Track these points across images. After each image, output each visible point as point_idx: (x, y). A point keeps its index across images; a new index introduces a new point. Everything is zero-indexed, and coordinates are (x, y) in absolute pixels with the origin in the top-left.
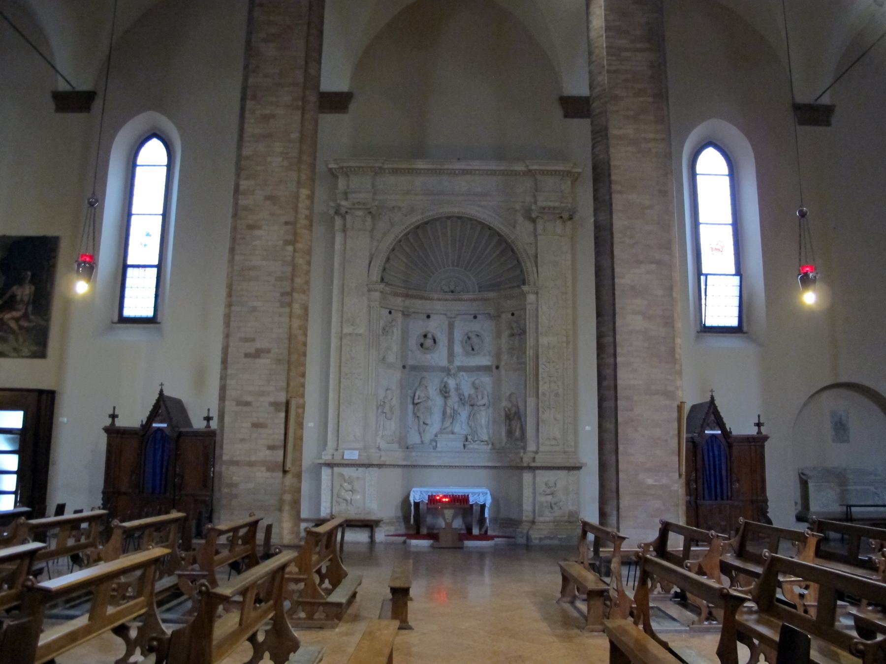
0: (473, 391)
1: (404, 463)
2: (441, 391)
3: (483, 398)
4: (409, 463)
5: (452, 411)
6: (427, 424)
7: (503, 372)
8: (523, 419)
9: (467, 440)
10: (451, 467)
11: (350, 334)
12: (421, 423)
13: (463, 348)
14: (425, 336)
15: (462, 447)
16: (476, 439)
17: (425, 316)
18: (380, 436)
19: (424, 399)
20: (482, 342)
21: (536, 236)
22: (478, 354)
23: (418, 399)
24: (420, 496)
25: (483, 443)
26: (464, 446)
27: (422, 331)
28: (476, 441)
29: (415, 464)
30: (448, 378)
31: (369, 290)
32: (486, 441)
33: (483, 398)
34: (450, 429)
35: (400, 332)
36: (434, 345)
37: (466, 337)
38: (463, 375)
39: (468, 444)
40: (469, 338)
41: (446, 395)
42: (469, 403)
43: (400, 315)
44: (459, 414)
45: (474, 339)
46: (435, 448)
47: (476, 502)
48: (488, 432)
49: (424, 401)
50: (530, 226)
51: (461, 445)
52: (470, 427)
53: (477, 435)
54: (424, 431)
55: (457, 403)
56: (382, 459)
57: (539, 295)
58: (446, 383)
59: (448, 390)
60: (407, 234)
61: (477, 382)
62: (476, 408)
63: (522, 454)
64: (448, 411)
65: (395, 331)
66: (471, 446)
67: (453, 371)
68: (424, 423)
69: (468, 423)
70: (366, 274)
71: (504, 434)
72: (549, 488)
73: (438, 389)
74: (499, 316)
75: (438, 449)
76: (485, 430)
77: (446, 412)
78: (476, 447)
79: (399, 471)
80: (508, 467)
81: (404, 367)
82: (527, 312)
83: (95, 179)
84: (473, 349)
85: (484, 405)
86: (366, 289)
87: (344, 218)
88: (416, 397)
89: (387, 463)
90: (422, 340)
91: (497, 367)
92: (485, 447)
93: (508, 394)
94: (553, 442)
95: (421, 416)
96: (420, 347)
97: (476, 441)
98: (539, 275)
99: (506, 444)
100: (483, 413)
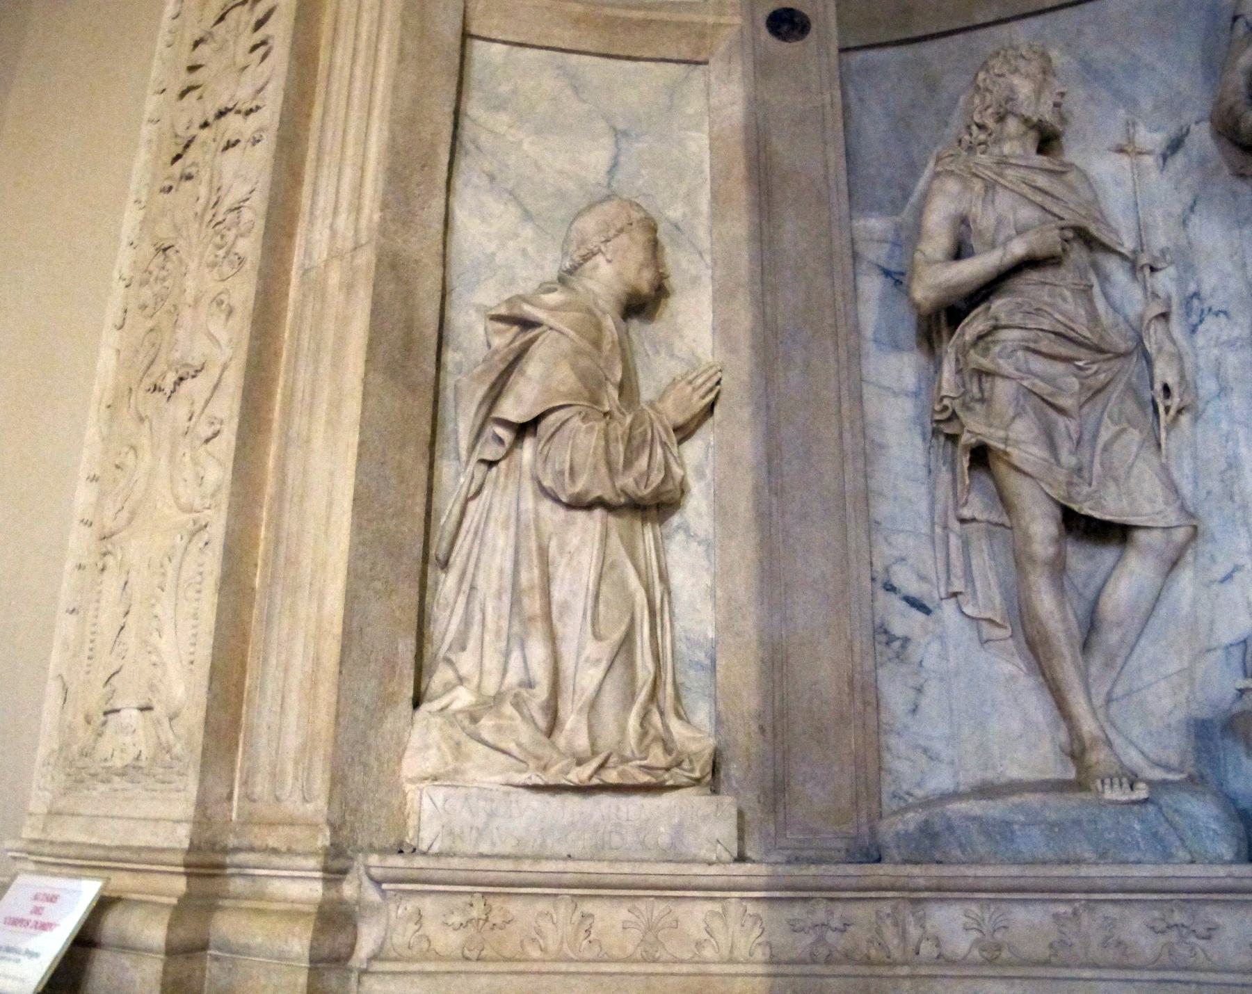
19: (1018, 249)
23: (959, 252)
54: (1091, 626)
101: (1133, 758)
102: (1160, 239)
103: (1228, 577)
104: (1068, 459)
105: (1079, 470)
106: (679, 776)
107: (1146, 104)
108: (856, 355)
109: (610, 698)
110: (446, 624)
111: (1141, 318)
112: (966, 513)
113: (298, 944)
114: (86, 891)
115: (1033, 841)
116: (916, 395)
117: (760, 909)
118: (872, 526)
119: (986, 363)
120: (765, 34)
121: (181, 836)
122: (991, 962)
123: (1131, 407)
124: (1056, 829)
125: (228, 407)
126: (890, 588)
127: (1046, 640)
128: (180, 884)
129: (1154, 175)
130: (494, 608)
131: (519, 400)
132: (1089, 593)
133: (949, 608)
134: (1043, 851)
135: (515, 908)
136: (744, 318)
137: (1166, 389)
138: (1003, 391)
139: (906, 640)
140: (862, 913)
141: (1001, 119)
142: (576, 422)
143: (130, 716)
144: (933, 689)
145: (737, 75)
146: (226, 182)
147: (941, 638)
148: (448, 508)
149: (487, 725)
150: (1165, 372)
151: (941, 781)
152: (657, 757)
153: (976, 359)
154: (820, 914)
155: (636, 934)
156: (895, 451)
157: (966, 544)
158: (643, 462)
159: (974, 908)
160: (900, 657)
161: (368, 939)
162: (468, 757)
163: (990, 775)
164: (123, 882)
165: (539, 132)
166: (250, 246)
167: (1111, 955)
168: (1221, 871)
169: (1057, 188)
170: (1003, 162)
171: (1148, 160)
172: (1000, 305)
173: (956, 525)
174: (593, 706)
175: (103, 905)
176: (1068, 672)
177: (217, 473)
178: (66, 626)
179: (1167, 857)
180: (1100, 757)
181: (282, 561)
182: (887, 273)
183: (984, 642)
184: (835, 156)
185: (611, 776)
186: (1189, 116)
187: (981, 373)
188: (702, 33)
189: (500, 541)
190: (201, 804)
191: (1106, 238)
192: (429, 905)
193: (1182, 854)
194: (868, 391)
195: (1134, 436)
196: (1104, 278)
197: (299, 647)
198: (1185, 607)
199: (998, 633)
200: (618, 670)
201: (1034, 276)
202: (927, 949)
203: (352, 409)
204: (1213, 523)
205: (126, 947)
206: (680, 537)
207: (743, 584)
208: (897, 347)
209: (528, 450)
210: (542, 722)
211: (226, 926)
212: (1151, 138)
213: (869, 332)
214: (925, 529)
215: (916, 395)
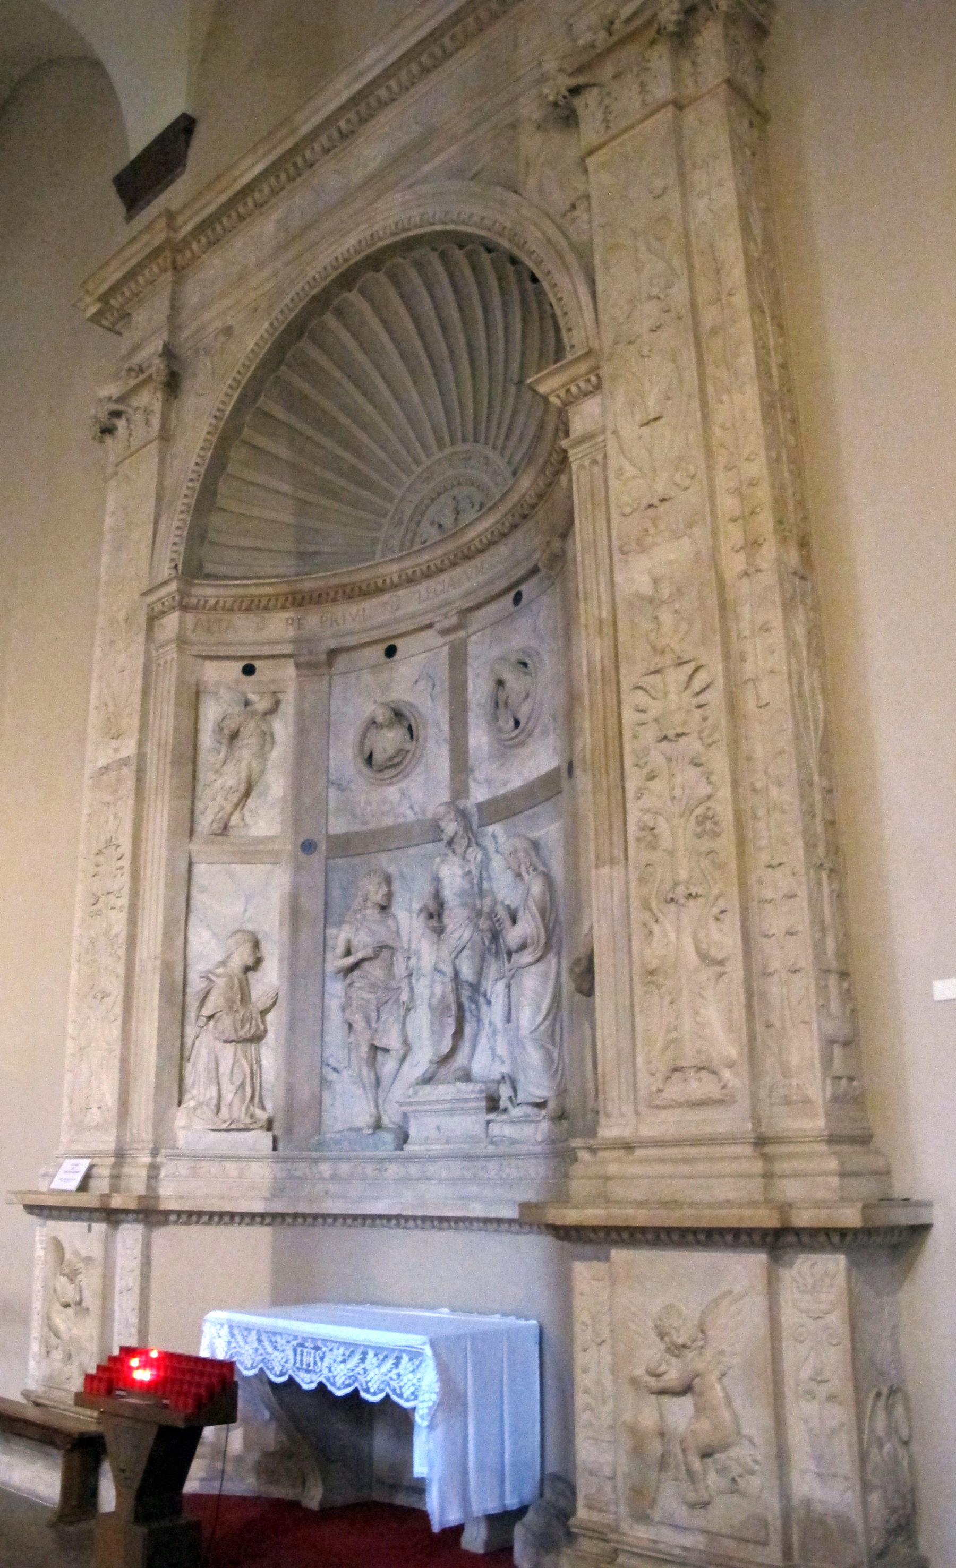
10: (442, 1222)
24: (229, 1343)
38: (494, 836)
43: (289, 671)
47: (387, 1397)
72: (677, 1350)
79: (262, 1234)
80: (263, 1216)
81: (308, 847)
94: (698, 1087)
98: (601, 305)
106: (255, 1126)
109: (237, 1102)
110: (189, 1080)
113: (144, 1173)
114: (84, 1164)
115: (346, 1144)
120: (300, 853)
121: (112, 1146)
125: (118, 1010)
126: (328, 1065)
128: (113, 1160)
130: (203, 1076)
135: (203, 1163)
143: (94, 1110)
148: (189, 1041)
149: (198, 1112)
152: (248, 1120)
158: (248, 1026)
161: (163, 1173)
164: (96, 1161)
166: (122, 952)
171: (415, 915)
174: (231, 1105)
175: (91, 1167)
177: (116, 1032)
178: (68, 1077)
185: (233, 1126)
189: (204, 1052)
190: (118, 1137)
192: (179, 1163)
200: (239, 1094)
203: (156, 1015)
205: (100, 1177)
209: (212, 1023)
211: (126, 1170)
212: (416, 906)
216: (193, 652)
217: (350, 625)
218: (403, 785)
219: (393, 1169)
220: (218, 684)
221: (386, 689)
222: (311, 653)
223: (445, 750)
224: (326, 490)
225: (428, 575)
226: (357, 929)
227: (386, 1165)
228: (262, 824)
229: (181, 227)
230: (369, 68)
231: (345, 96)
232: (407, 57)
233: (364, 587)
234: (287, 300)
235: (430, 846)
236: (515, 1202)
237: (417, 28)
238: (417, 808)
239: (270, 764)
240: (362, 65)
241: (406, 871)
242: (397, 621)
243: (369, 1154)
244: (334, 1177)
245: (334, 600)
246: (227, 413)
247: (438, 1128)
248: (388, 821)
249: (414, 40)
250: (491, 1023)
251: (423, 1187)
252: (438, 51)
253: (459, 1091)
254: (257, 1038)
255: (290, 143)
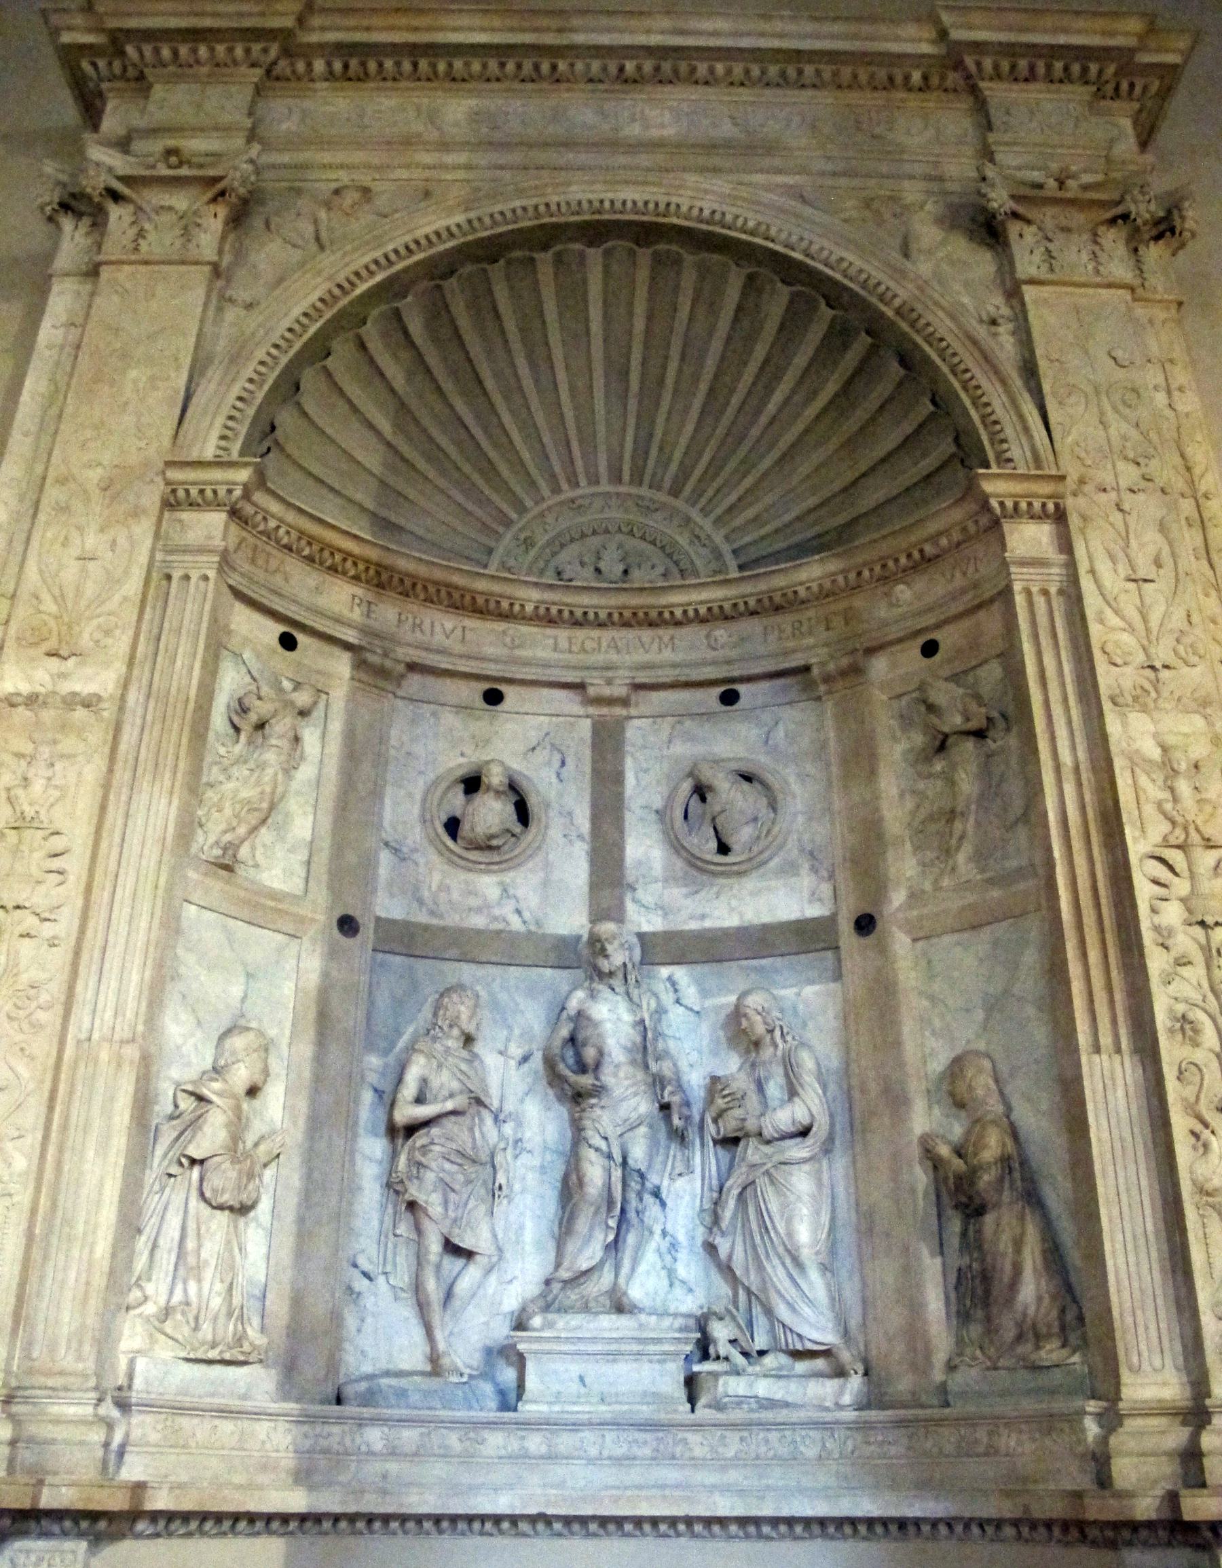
0: (731, 1065)
1: (296, 1501)
2: (550, 1063)
3: (792, 1093)
4: (330, 1502)
5: (617, 1174)
6: (468, 1255)
7: (901, 943)
8: (1057, 1193)
9: (704, 1349)
11: (32, 700)
12: (435, 1246)
13: (676, 846)
14: (472, 784)
15: (681, 1393)
16: (761, 1342)
17: (472, 692)
18: (150, 1309)
19: (449, 1105)
20: (773, 806)
21: (1013, 293)
22: (754, 864)
23: (420, 1100)
25: (801, 1366)
26: (691, 1382)
27: (458, 762)
28: (761, 1353)
29: (371, 1505)
30: (593, 995)
31: (171, 503)
32: (827, 1353)
33: (792, 1093)
34: (606, 1279)
35: (335, 747)
36: (518, 828)
37: (687, 786)
38: (671, 980)
39: (715, 1375)
40: (701, 792)
41: (586, 1081)
42: (711, 1128)
43: (341, 666)
44: (656, 1194)
45: (728, 792)
46: (510, 1399)
48: (836, 1300)
49: (454, 1113)
50: (983, 263)
51: (670, 1381)
52: (726, 1270)
53: (769, 1312)
54: (449, 1295)
55: (643, 1130)
56: (132, 1471)
57: (1074, 521)
58: (580, 1016)
59: (590, 1054)
60: (393, 289)
61: (755, 1001)
62: (752, 1151)
63: (1092, 1428)
64: (595, 1172)
65: (310, 737)
66: (734, 1386)
67: (617, 957)
68: (452, 1249)
69: (711, 1248)
70: (171, 432)
71: (935, 1302)
73: (538, 1058)
74: (855, 671)
75: (528, 1409)
76: (816, 1284)
77: (581, 1184)
78: (763, 1388)
81: (347, 925)
82: (1020, 600)
83: (155, 1240)
84: (723, 849)
85: (804, 1132)
86: (152, 497)
87: (98, 220)
88: (409, 1089)
89: (160, 1501)
90: (456, 801)
91: (865, 924)
92: (825, 1389)
93: (938, 1065)
95: (432, 1202)
96: (441, 831)
97: (761, 1353)
99: (951, 1367)
100: (801, 1182)
101: (460, 1364)
102: (509, 1107)
103: (510, 1282)
104: (451, 1214)
105: (455, 1221)
107: (517, 1032)
108: (355, 1136)
111: (495, 1147)
112: (398, 1232)
115: (415, 1398)
116: (381, 1163)
117: (292, 1426)
118: (351, 1231)
119: (423, 1160)
120: (336, 931)
122: (393, 1453)
123: (483, 1191)
124: (427, 1394)
126: (355, 1266)
127: (428, 1304)
129: (513, 1072)
131: (198, 1146)
132: (449, 1281)
133: (382, 1279)
134: (419, 1404)
136: (303, 1106)
137: (500, 1188)
138: (430, 1177)
139: (359, 1294)
140: (336, 1429)
141: (451, 1026)
142: (227, 1165)
144: (369, 1320)
145: (319, 950)
146: (22, 967)
147: (376, 1295)
150: (501, 1179)
151: (367, 1368)
153: (418, 1156)
154: (318, 1429)
155: (236, 1437)
156: (367, 1192)
157: (395, 1246)
159: (386, 1430)
160: (355, 1302)
162: (156, 1341)
163: (391, 1367)
165: (210, 969)
167: (442, 1451)
168: (492, 1414)
169: (471, 1073)
170: (447, 1050)
171: (513, 1063)
172: (435, 1131)
173: (391, 1236)
174: (215, 1319)
176: (436, 1319)
179: (470, 1408)
180: (445, 1361)
181: (58, 1221)
182: (376, 1090)
183: (396, 1299)
184: (361, 1015)
186: (534, 1046)
187: (419, 1165)
188: (301, 920)
191: (487, 1101)
193: (475, 1405)
194: (358, 1158)
195: (483, 1209)
196: (482, 1120)
197: (72, 1275)
198: (490, 1291)
199: (404, 1295)
201: (453, 1118)
202: (364, 1448)
204: (508, 1255)
206: (253, 1225)
207: (285, 1254)
208: (376, 1135)
210: (193, 1324)
212: (516, 1051)
213: (362, 1123)
214: (376, 1236)
215: (381, 1163)
216: (231, 582)
217: (439, 639)
218: (508, 877)
219: (495, 1441)
220: (246, 641)
221: (482, 742)
222: (386, 655)
223: (581, 851)
224: (435, 454)
225: (577, 623)
226: (440, 1066)
227: (486, 1434)
228: (277, 871)
229: (313, 30)
230: (699, 33)
231: (655, 40)
232: (756, 54)
233: (480, 600)
234: (506, 207)
235: (549, 972)
236: (1166, 1453)
237: (781, 36)
238: (527, 915)
239: (295, 785)
240: (694, 24)
241: (503, 997)
242: (514, 661)
243: (461, 1414)
244: (393, 1453)
245: (428, 600)
246: (358, 292)
247: (582, 1379)
248: (478, 921)
249: (776, 43)
250: (664, 1233)
251: (558, 1471)
252: (756, 71)
253: (641, 1326)
254: (243, 1210)
255: (549, 39)
